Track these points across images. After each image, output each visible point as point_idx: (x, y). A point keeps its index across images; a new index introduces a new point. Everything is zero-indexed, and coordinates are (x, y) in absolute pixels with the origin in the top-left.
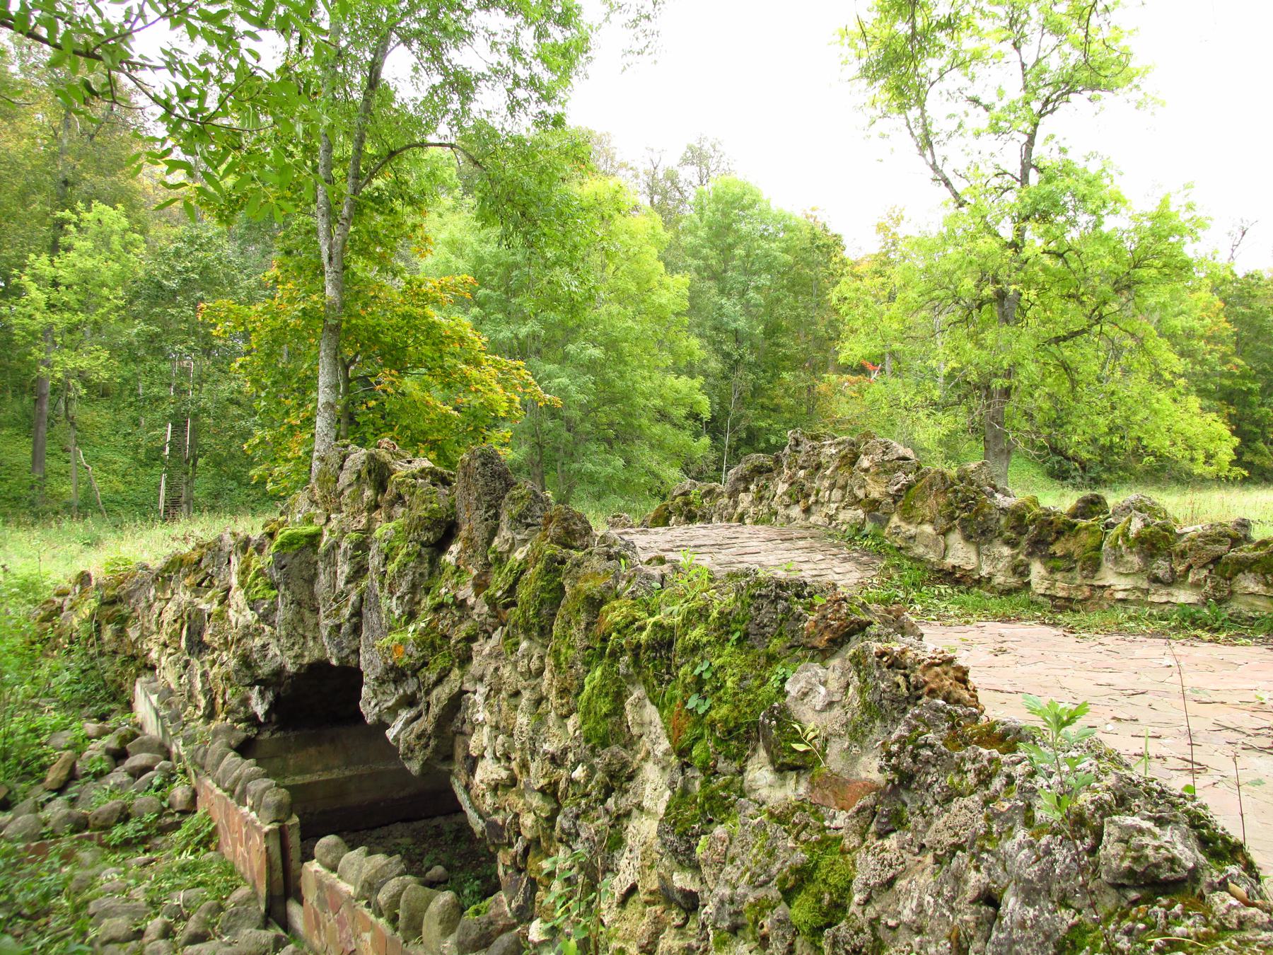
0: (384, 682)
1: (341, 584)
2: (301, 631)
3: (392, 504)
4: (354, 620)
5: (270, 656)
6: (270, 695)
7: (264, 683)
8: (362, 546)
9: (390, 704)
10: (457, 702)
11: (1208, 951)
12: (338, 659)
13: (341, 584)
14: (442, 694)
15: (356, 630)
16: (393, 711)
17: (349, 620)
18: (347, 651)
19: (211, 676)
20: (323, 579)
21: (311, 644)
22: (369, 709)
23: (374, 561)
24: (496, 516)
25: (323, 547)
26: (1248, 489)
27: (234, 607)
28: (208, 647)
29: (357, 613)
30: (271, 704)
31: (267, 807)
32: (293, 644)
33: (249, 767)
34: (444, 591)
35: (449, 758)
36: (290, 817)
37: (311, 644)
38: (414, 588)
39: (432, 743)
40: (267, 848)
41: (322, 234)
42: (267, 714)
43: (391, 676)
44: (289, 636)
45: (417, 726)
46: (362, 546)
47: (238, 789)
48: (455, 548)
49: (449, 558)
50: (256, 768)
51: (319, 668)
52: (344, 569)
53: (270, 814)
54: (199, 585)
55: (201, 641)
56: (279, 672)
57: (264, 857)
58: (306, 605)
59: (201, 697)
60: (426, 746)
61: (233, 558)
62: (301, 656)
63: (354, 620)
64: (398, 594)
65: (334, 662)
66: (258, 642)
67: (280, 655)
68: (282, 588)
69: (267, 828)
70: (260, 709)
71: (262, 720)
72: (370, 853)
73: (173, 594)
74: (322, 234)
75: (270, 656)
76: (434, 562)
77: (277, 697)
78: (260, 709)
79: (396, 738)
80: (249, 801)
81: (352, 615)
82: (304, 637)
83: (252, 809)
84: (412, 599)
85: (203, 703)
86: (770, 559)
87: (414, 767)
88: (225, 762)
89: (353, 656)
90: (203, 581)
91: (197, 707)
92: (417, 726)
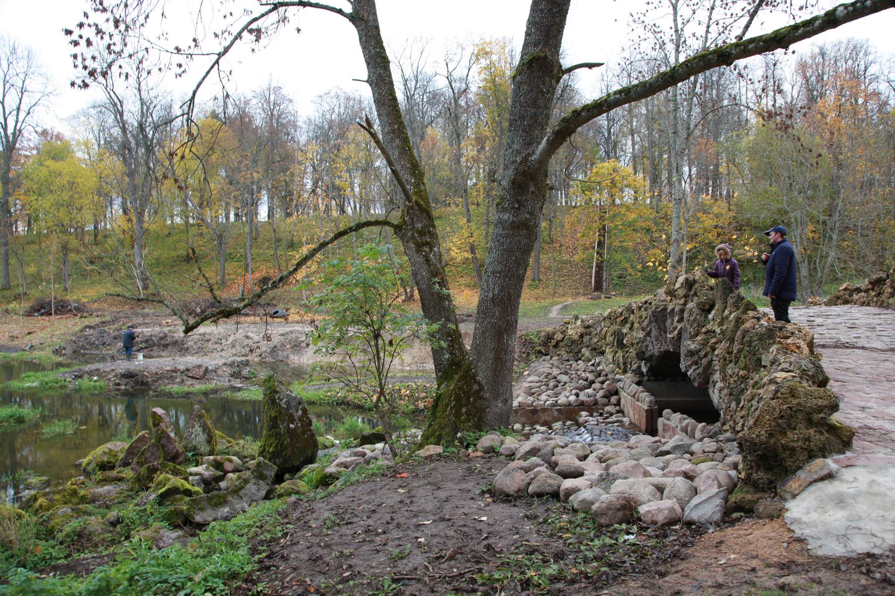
3: (693, 296)
6: (648, 365)
7: (648, 360)
8: (682, 311)
10: (710, 362)
11: (803, 3)
14: (704, 361)
16: (690, 366)
20: (669, 321)
22: (682, 367)
23: (686, 315)
24: (726, 302)
26: (774, 32)
33: (641, 388)
34: (709, 327)
35: (708, 383)
41: (7, 354)
45: (698, 371)
46: (682, 311)
48: (713, 312)
49: (710, 316)
51: (666, 353)
52: (676, 319)
55: (622, 343)
56: (651, 356)
67: (655, 349)
74: (7, 354)
76: (706, 317)
77: (651, 366)
85: (622, 367)
87: (696, 384)
92: (698, 371)
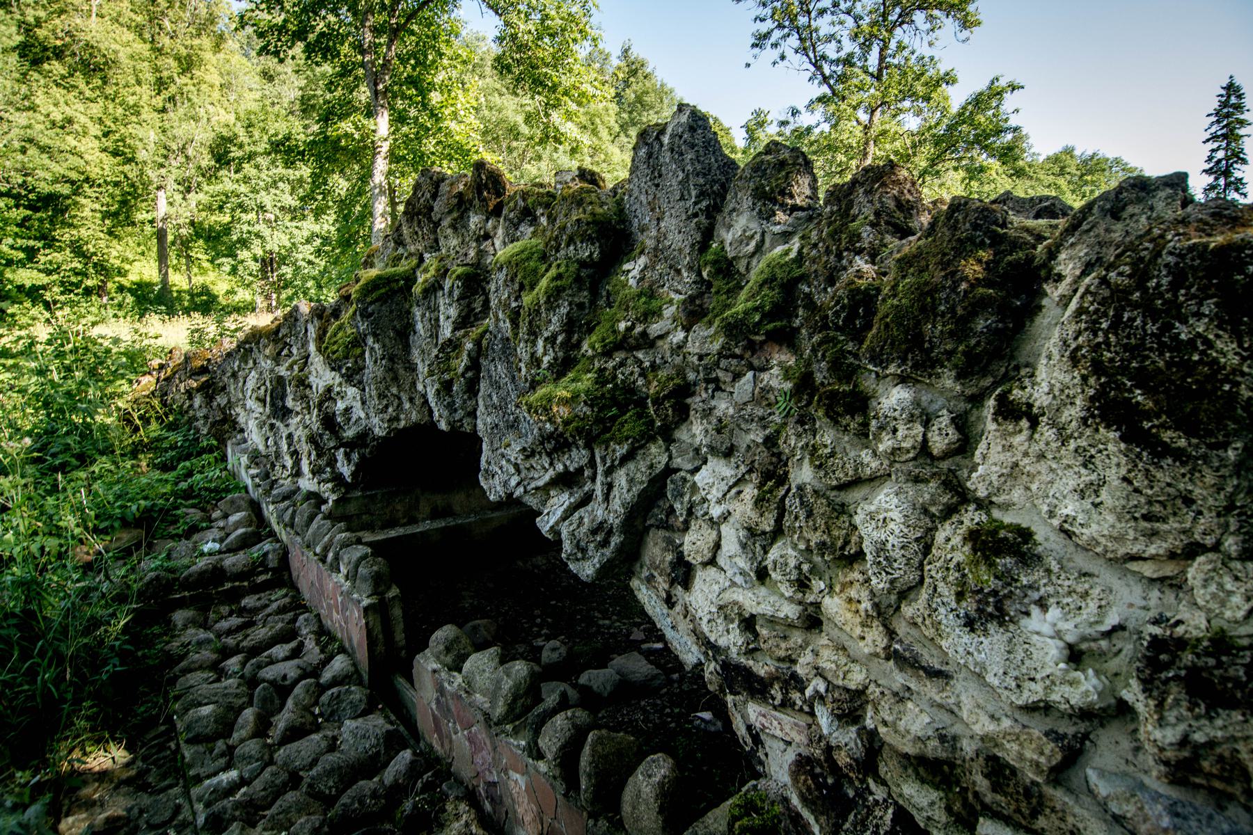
0: (533, 454)
1: (446, 332)
2: (394, 390)
4: (469, 374)
5: (353, 420)
6: (355, 457)
7: (350, 445)
9: (541, 483)
12: (449, 423)
13: (446, 332)
15: (472, 389)
17: (463, 375)
18: (460, 413)
19: (296, 438)
21: (407, 406)
25: (417, 289)
27: (314, 373)
28: (291, 411)
29: (474, 365)
30: (357, 465)
31: (364, 579)
32: (387, 407)
36: (389, 588)
37: (407, 406)
38: (570, 325)
39: (616, 540)
40: (367, 624)
42: (353, 474)
43: (549, 446)
44: (381, 396)
47: (331, 555)
50: (348, 534)
52: (448, 312)
53: (367, 587)
54: (279, 354)
55: (284, 407)
56: (363, 437)
57: (364, 632)
58: (398, 363)
59: (287, 458)
60: (605, 543)
61: (310, 327)
62: (397, 419)
63: (469, 374)
64: (546, 334)
65: (443, 426)
66: (341, 405)
68: (370, 340)
69: (366, 602)
70: (346, 470)
71: (349, 480)
72: (503, 660)
73: (255, 363)
75: (353, 420)
78: (346, 470)
79: (555, 530)
80: (343, 570)
81: (467, 369)
82: (399, 399)
83: (347, 578)
84: (568, 339)
86: (544, 390)
88: (314, 525)
89: (469, 420)
90: (282, 350)
91: (284, 467)
